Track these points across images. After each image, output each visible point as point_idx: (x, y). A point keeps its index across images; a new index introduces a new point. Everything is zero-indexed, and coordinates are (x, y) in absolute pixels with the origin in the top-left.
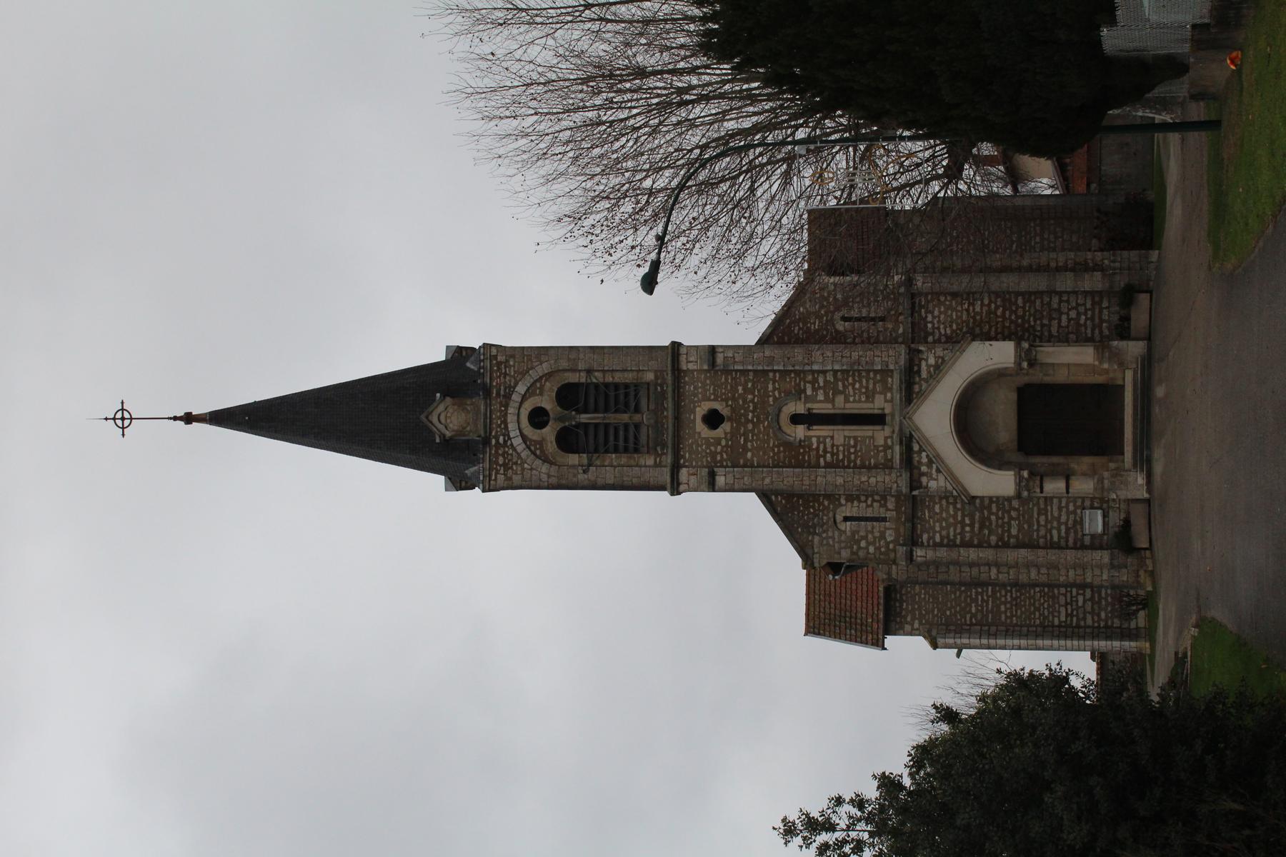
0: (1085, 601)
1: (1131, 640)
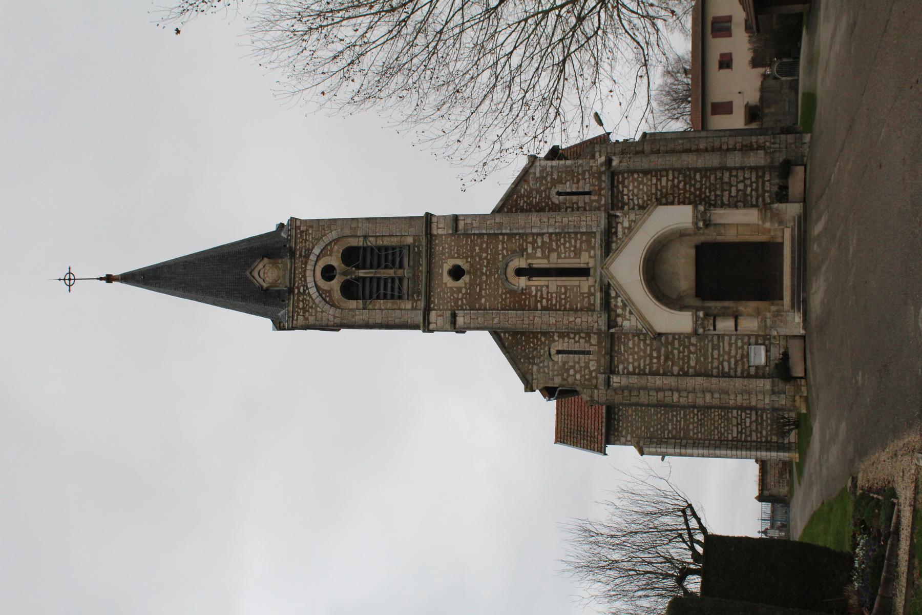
0: (751, 423)
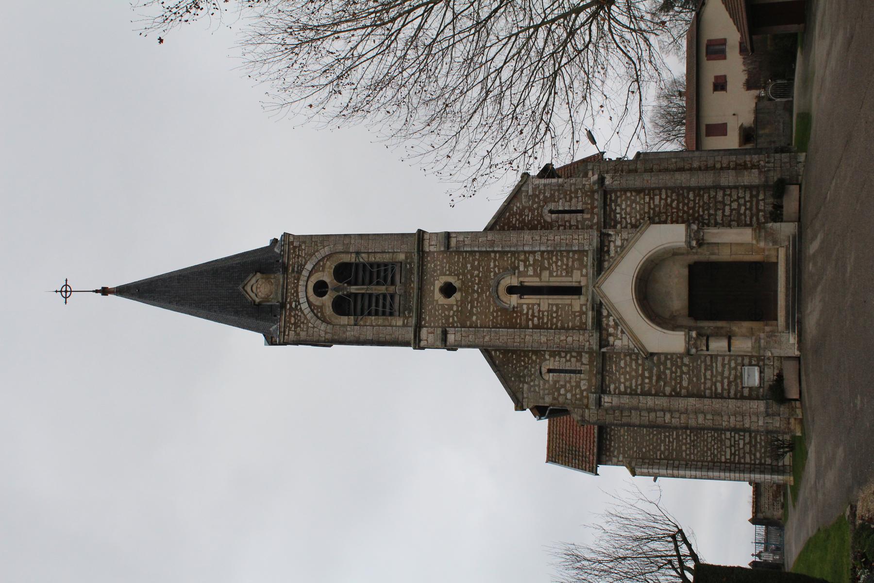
0: (744, 444)
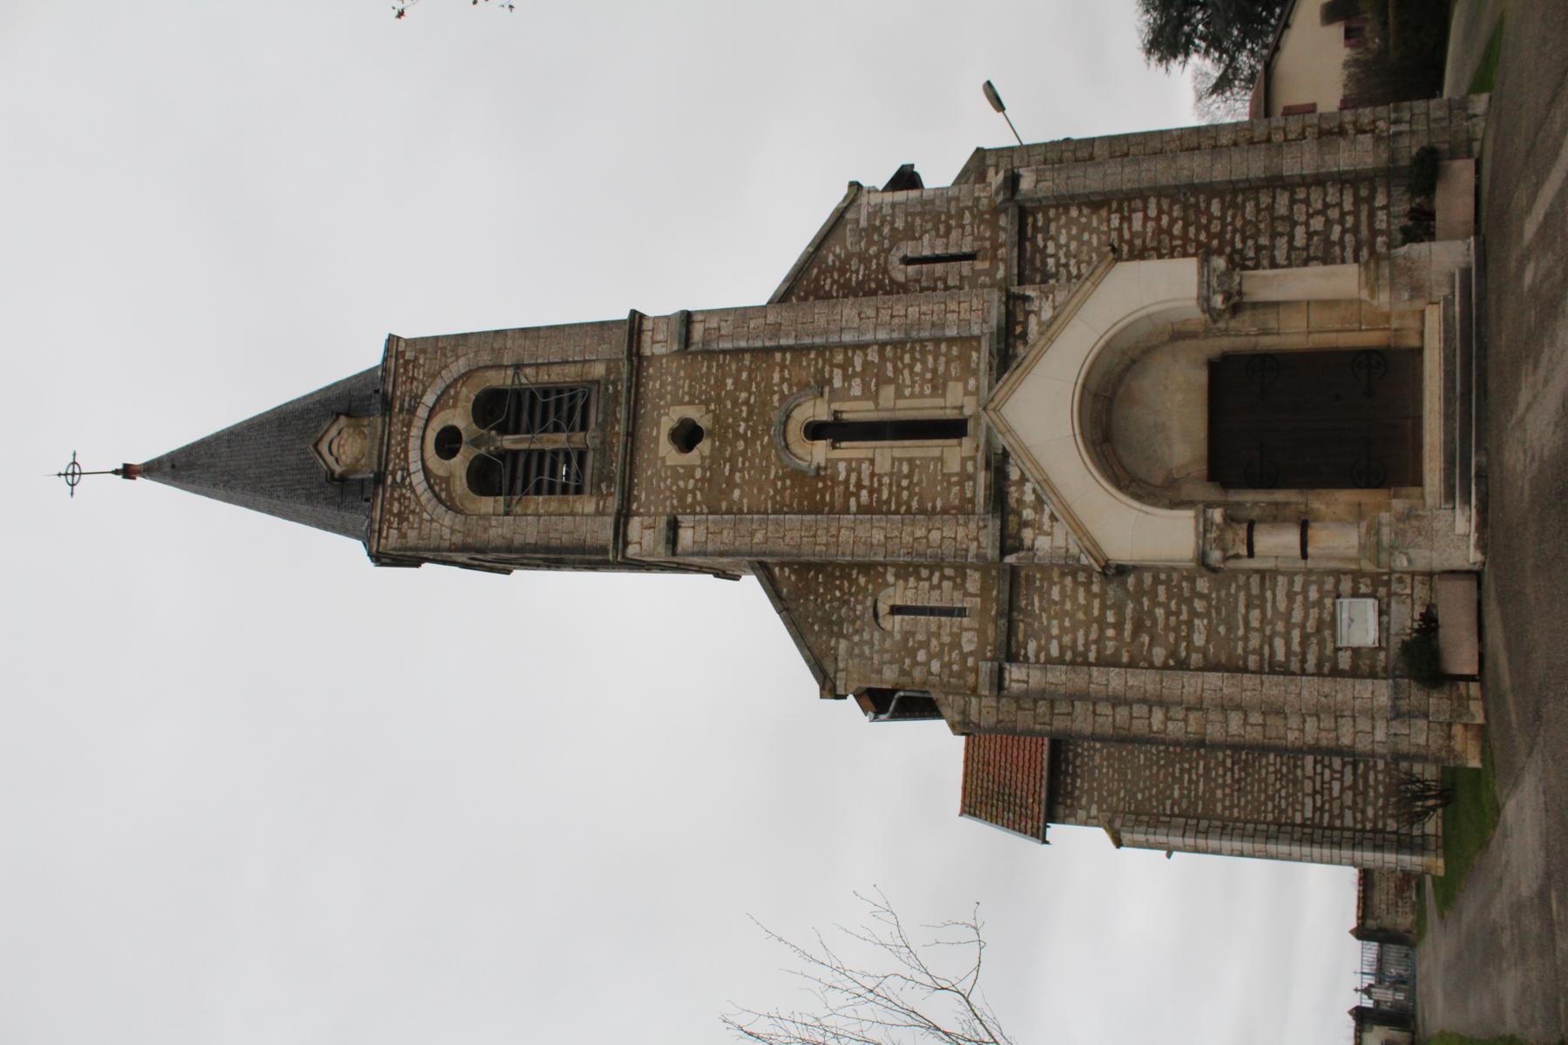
0: (1342, 790)
1: (1412, 854)
